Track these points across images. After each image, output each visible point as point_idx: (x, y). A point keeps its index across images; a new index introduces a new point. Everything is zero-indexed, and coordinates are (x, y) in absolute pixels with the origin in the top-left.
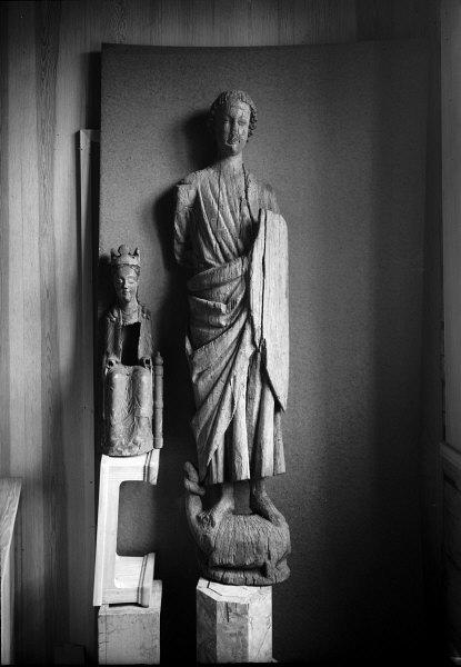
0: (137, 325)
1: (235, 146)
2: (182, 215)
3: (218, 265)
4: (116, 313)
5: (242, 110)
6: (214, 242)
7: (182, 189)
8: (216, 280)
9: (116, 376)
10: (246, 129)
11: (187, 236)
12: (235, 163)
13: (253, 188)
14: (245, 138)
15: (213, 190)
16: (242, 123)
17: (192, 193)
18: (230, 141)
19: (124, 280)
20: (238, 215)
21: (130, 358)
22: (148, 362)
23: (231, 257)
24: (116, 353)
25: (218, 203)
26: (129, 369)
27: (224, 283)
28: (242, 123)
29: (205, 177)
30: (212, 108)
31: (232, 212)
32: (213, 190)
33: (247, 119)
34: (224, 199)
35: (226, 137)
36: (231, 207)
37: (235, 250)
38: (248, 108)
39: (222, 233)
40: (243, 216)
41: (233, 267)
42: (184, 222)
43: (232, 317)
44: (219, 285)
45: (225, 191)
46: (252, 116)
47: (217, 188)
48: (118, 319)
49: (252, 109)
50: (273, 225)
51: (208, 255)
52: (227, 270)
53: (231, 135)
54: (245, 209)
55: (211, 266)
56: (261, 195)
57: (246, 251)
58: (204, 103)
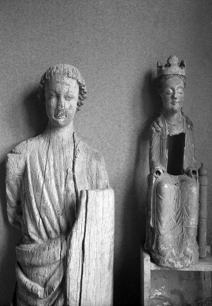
0: (182, 135)
1: (61, 121)
2: (12, 183)
3: (40, 241)
4: (161, 124)
5: (69, 86)
6: (38, 218)
7: (12, 158)
8: (35, 261)
9: (166, 186)
10: (74, 103)
11: (19, 202)
12: (65, 134)
13: (81, 157)
14: (72, 112)
15: (40, 162)
16: (68, 97)
17: (21, 164)
18: (56, 116)
19: (174, 90)
20: (62, 190)
21: (175, 168)
22: (194, 172)
23: (53, 235)
24: (162, 162)
25: (44, 176)
26: (175, 178)
27: (42, 265)
28: (68, 97)
29: (34, 147)
30: (41, 83)
31: (57, 186)
32: (40, 158)
33: (75, 92)
34: (50, 172)
35: (53, 112)
36: (56, 181)
37: (57, 228)
38: (74, 82)
39: (45, 209)
40: (67, 190)
41: (52, 250)
42: (15, 188)
43: (51, 300)
44: (38, 266)
45: (52, 163)
46: (81, 89)
47: (44, 160)
48: (164, 129)
49: (79, 83)
50: (96, 204)
51: (31, 228)
52: (45, 253)
53: (57, 110)
54: (71, 182)
55: (32, 241)
56: (90, 163)
57: (67, 232)
58: (34, 79)
